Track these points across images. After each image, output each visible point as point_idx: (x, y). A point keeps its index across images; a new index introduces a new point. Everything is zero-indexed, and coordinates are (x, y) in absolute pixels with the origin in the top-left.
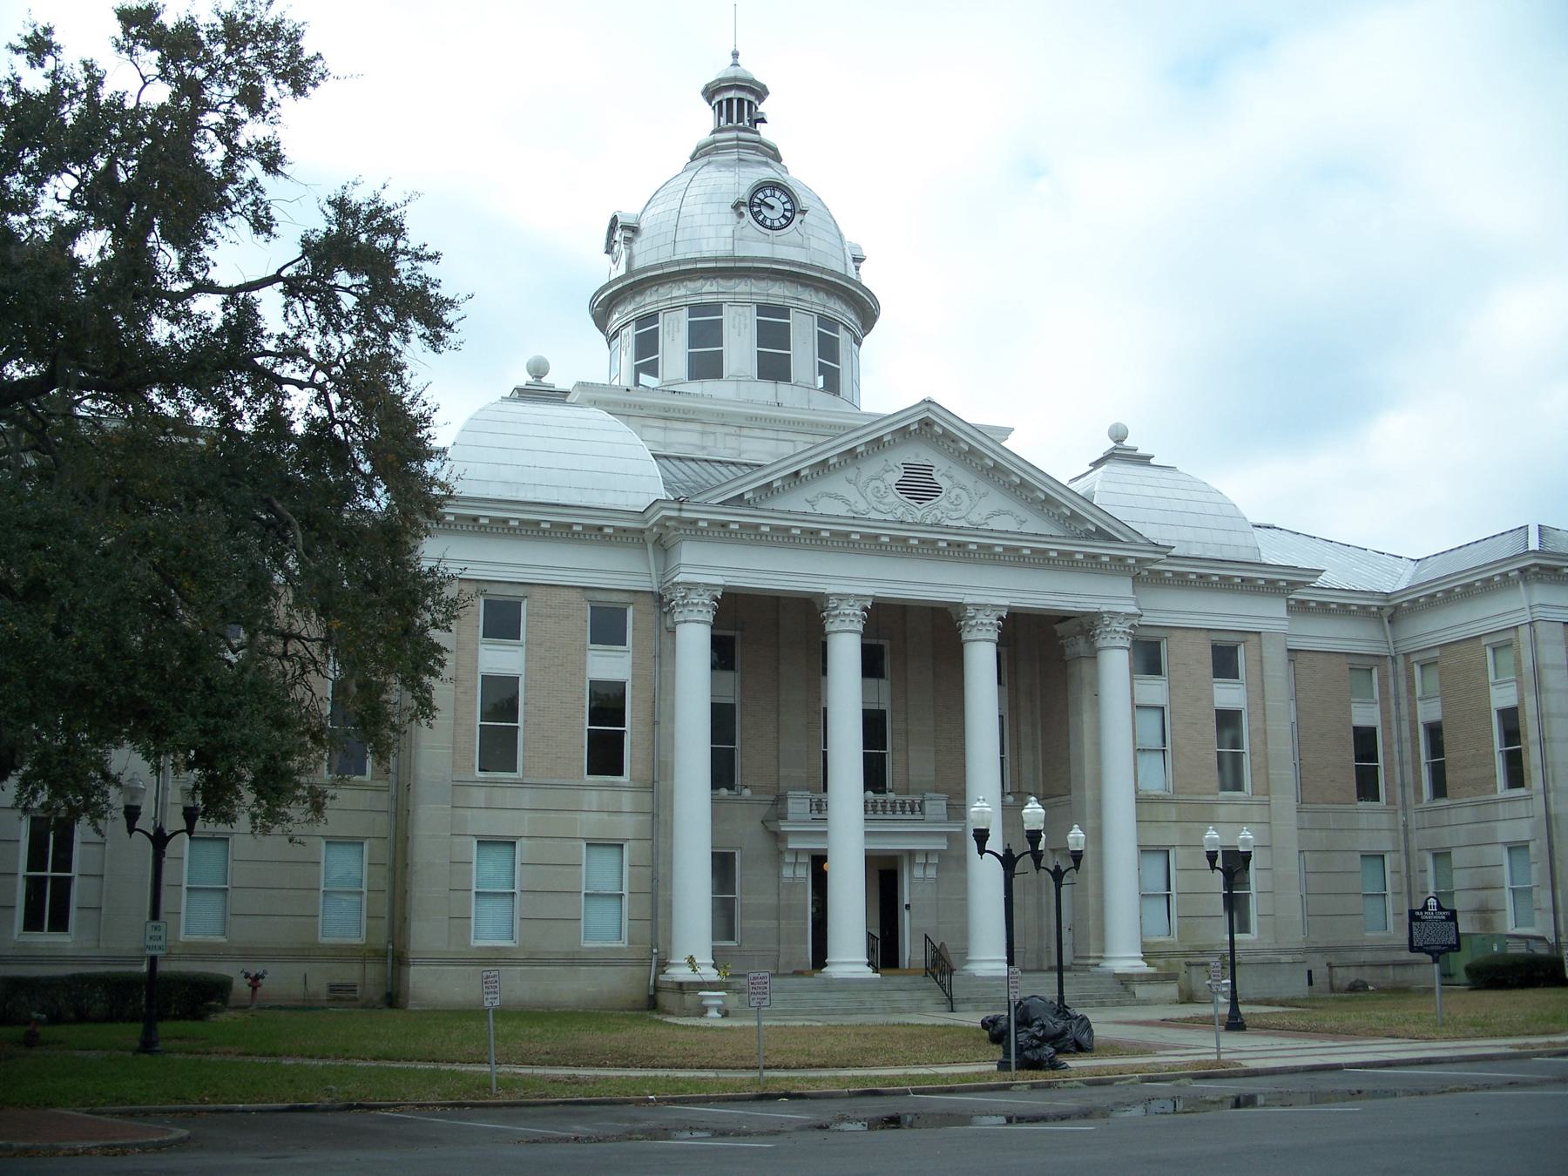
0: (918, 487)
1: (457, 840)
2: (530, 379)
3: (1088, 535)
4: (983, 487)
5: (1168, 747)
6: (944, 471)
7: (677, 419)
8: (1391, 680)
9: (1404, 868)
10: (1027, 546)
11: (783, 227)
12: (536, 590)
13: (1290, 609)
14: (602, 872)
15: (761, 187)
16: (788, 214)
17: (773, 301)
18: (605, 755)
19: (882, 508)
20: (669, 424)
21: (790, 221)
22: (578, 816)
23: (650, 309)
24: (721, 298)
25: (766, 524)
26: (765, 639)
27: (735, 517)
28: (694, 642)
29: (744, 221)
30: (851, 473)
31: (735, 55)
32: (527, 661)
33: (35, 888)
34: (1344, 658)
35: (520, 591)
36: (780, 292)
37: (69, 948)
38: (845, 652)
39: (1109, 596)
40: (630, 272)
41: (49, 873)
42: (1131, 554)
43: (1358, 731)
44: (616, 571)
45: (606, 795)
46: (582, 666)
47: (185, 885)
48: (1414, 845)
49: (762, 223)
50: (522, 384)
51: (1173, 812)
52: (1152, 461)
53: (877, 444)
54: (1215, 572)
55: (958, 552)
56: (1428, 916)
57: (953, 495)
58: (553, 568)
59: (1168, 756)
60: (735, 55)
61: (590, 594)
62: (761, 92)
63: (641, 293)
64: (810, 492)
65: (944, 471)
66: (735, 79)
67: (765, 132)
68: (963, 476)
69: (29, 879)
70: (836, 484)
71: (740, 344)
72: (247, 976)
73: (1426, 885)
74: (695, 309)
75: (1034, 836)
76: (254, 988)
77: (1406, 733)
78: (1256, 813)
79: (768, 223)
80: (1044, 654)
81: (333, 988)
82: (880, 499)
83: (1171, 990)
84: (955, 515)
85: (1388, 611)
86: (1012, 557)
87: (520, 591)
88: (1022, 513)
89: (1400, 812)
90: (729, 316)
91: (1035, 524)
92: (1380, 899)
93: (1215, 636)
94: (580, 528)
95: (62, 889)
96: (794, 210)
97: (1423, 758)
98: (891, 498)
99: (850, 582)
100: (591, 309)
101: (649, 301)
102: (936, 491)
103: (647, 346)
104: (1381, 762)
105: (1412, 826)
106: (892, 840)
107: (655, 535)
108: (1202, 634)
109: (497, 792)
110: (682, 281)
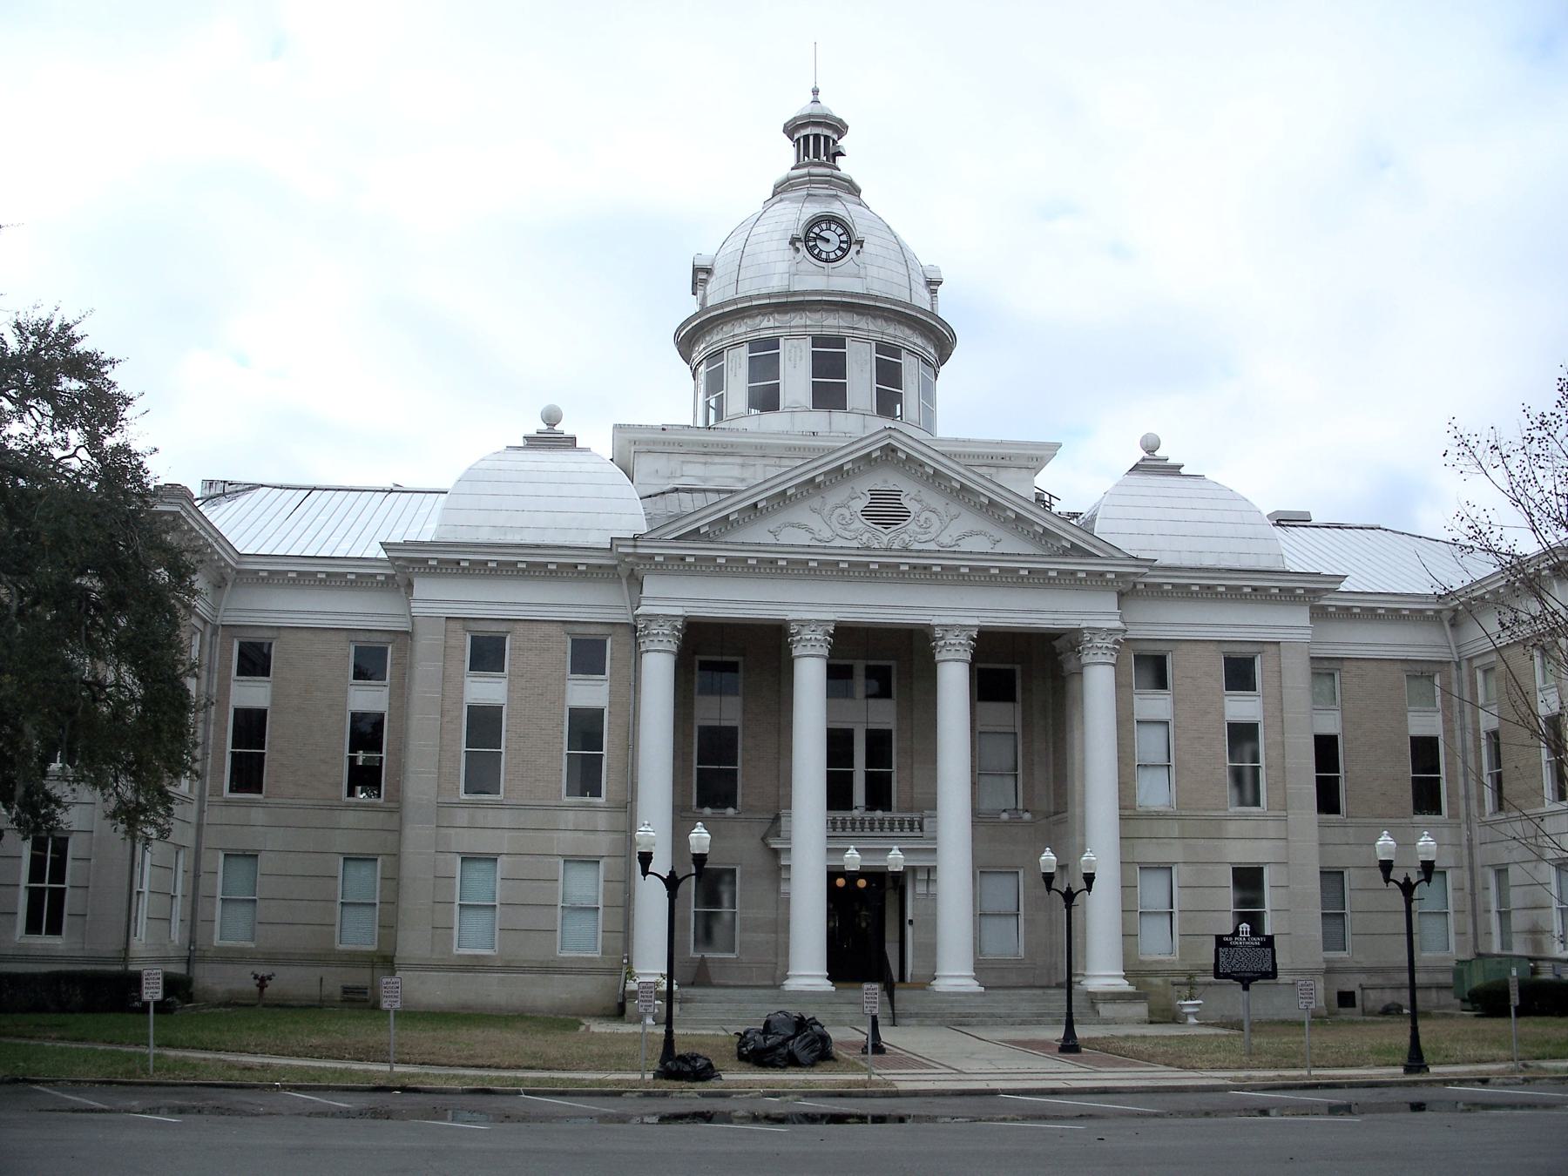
0: (886, 512)
1: (442, 856)
2: (544, 427)
3: (1065, 553)
4: (954, 509)
5: (1172, 762)
6: (912, 495)
7: (717, 454)
9: (1467, 885)
10: (994, 566)
14: (585, 886)
15: (817, 221)
17: (826, 332)
18: (586, 778)
19: (847, 534)
20: (709, 459)
21: (845, 252)
22: (555, 834)
23: (716, 347)
24: (778, 332)
25: (721, 554)
26: (738, 661)
27: (691, 550)
28: (658, 671)
29: (800, 255)
30: (816, 502)
31: (816, 92)
33: (35, 897)
34: (1399, 665)
35: (503, 627)
36: (835, 323)
37: (58, 949)
38: (810, 675)
39: (1090, 613)
40: (704, 309)
41: (46, 885)
43: (1416, 741)
44: (591, 605)
45: (583, 816)
47: (219, 896)
48: (1478, 861)
49: (817, 257)
50: (533, 432)
51: (1175, 828)
52: (1183, 471)
53: (839, 474)
54: (1221, 583)
55: (922, 574)
56: (1239, 941)
57: (922, 519)
59: (1173, 770)
60: (816, 92)
61: (569, 627)
62: (840, 128)
63: (709, 332)
64: (773, 523)
65: (912, 495)
66: (810, 116)
67: (845, 166)
68: (935, 500)
69: (32, 891)
70: (801, 514)
71: (796, 376)
72: (256, 977)
73: (1488, 903)
74: (755, 345)
75: (700, 859)
77: (1470, 743)
78: (1271, 828)
79: (824, 256)
80: (1025, 673)
81: (346, 990)
82: (845, 526)
83: (1141, 1009)
84: (924, 538)
85: (1447, 615)
86: (979, 576)
87: (503, 627)
88: (998, 533)
89: (1464, 826)
90: (785, 348)
91: (1011, 544)
92: (165, 924)
93: (1227, 648)
95: (58, 897)
96: (850, 241)
97: (1486, 770)
98: (857, 525)
99: (814, 609)
100: (677, 344)
101: (717, 339)
102: (902, 515)
103: (715, 383)
105: (1476, 841)
106: (922, 857)
107: (624, 566)
108: (1212, 647)
109: (480, 813)
110: (743, 318)
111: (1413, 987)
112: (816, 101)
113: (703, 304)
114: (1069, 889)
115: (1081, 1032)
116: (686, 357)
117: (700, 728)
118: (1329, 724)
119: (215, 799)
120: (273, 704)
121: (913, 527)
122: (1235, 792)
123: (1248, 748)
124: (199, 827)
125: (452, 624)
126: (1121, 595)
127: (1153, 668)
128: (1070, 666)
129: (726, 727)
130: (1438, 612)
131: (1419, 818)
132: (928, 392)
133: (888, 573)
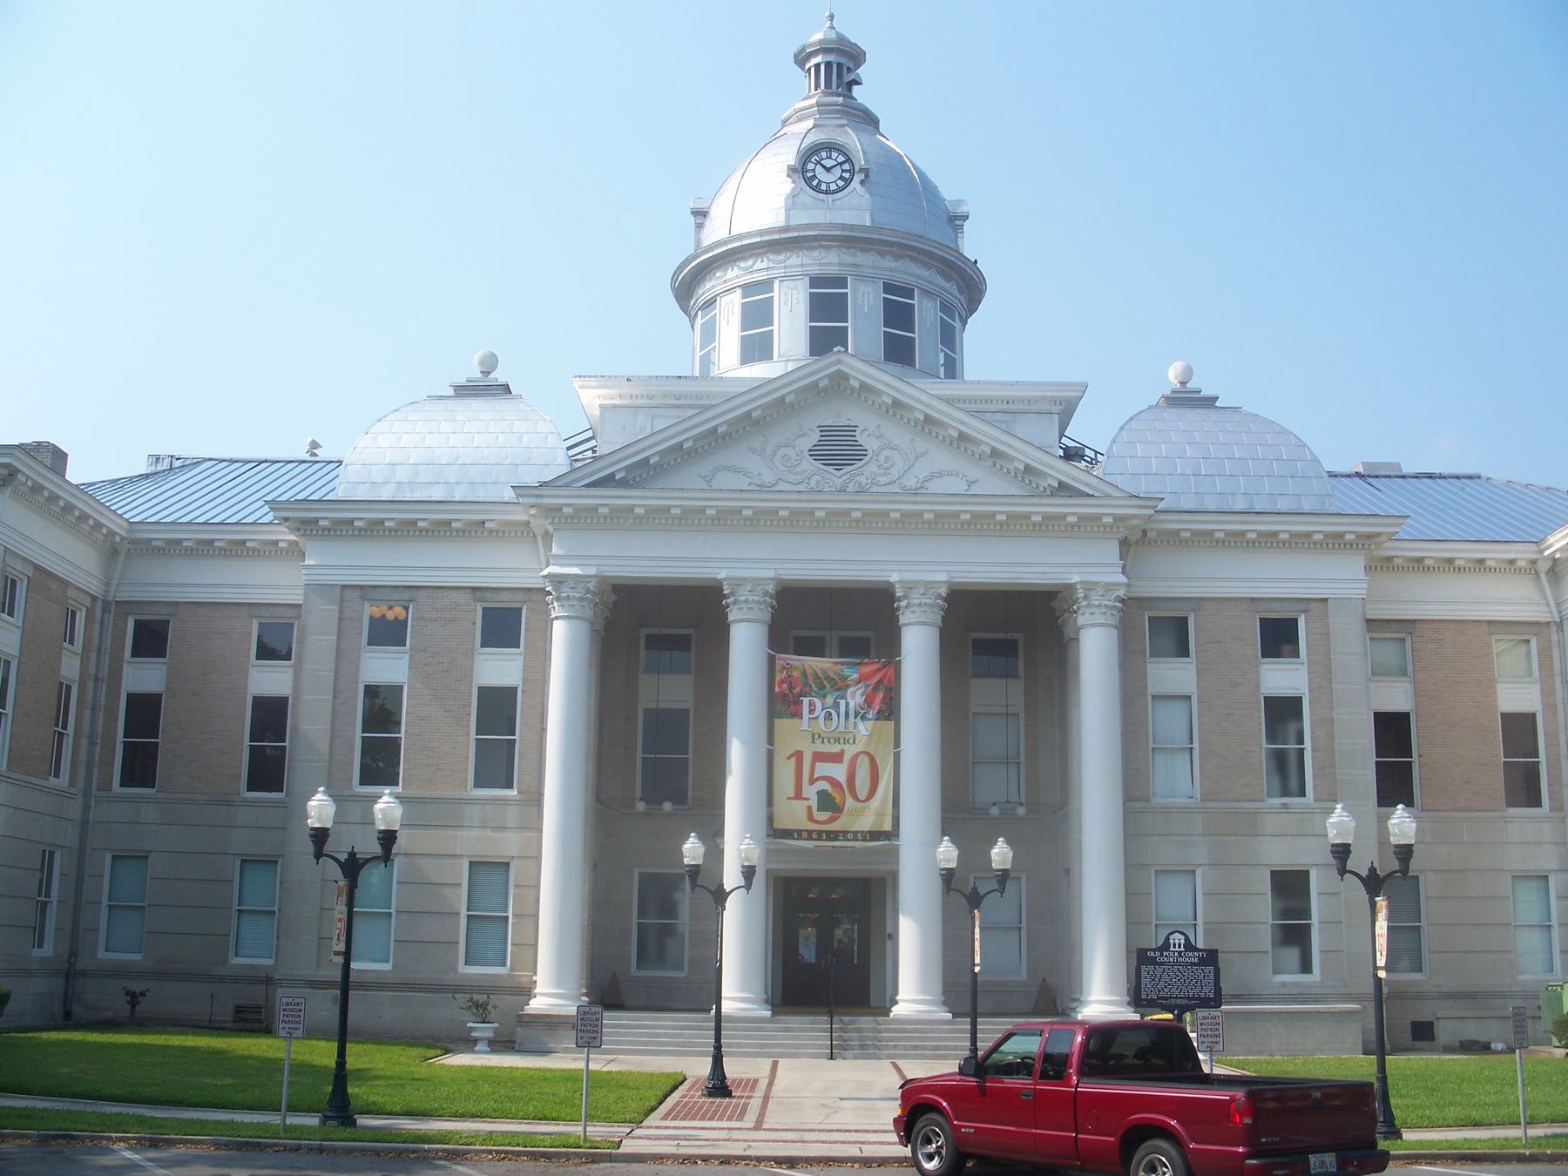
5: (1196, 745)
8: (1556, 653)
11: (840, 190)
12: (422, 594)
13: (1368, 569)
16: (847, 175)
19: (793, 478)
21: (848, 182)
28: (564, 643)
32: (1258, 679)
39: (1085, 567)
42: (1108, 511)
46: (469, 670)
49: (817, 189)
50: (462, 381)
55: (874, 523)
57: (882, 459)
58: (399, 568)
59: (1196, 753)
68: (898, 436)
74: (748, 289)
76: (133, 1007)
79: (823, 187)
81: (239, 1010)
84: (883, 480)
85: (1543, 567)
91: (990, 483)
94: (1222, 535)
102: (858, 454)
104: (1542, 758)
111: (345, 984)
112: (832, 28)
113: (698, 245)
114: (975, 889)
115: (732, 1069)
116: (686, 311)
117: (645, 710)
118: (1396, 698)
119: (103, 794)
120: (168, 688)
121: (872, 467)
122: (1276, 780)
123: (1292, 728)
124: (84, 824)
125: (348, 593)
126: (1124, 543)
127: (1163, 629)
128: (1068, 632)
129: (669, 710)
130: (1534, 562)
131: (1512, 811)
132: (949, 338)
133: (836, 523)
